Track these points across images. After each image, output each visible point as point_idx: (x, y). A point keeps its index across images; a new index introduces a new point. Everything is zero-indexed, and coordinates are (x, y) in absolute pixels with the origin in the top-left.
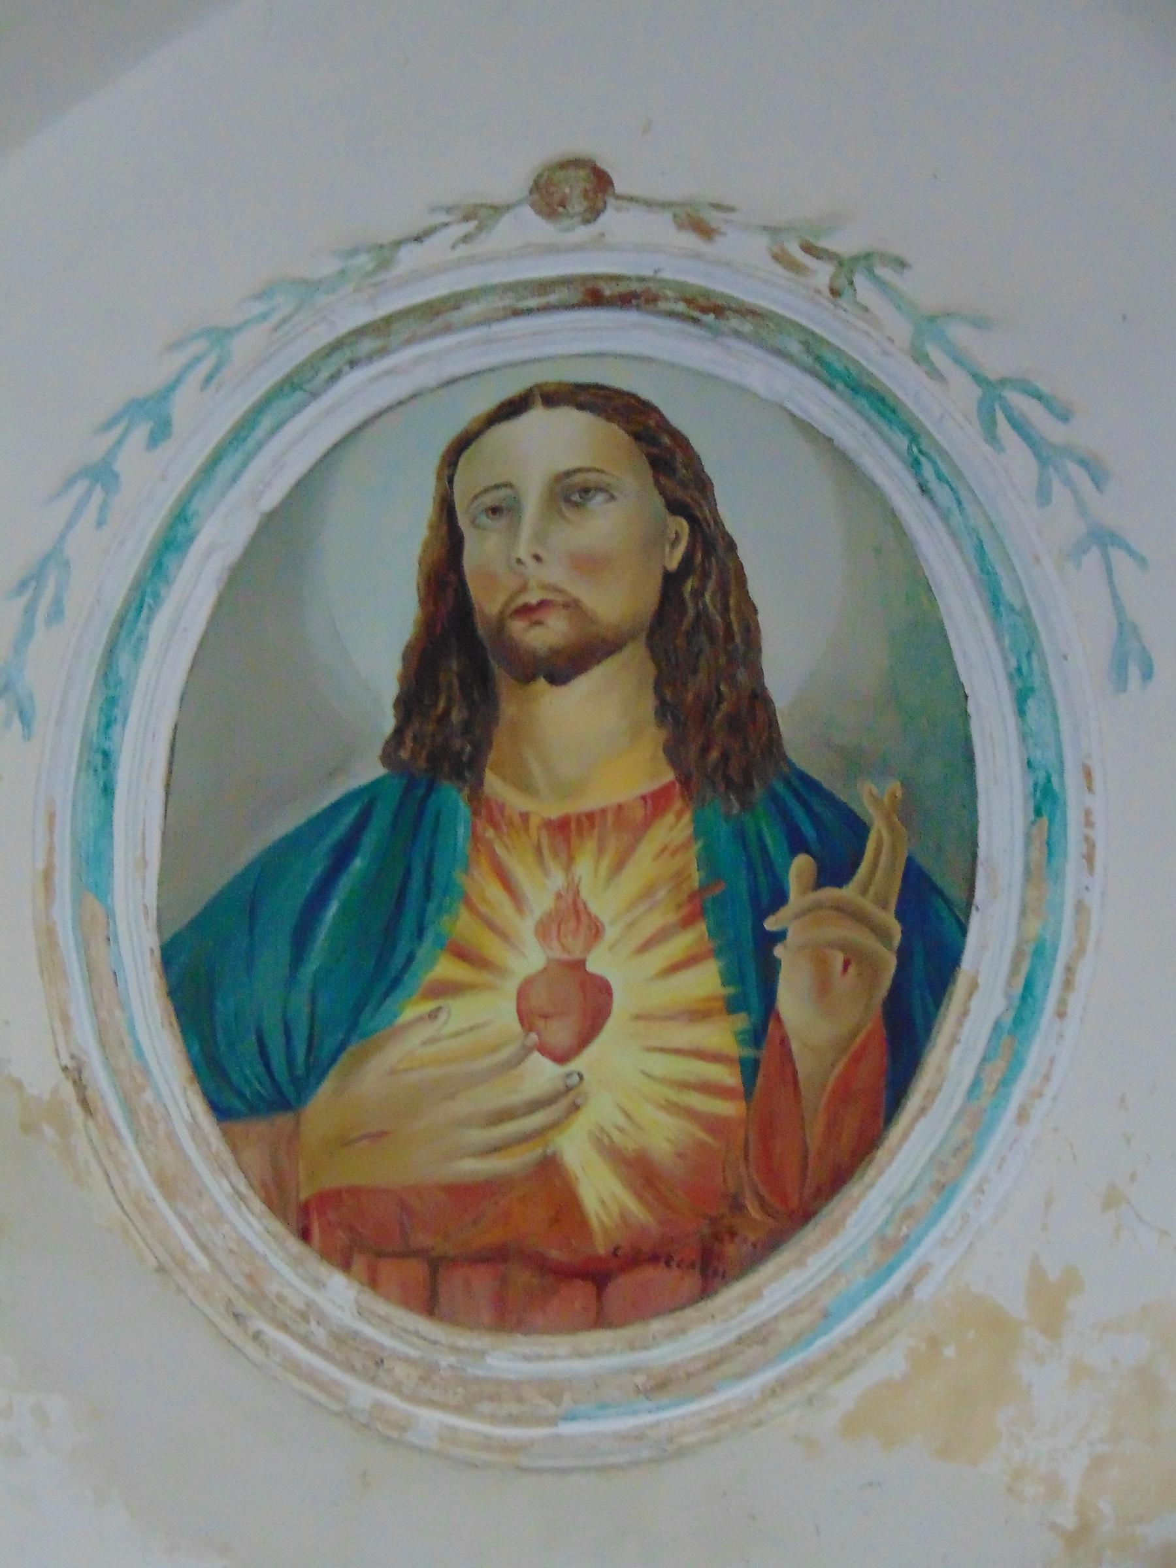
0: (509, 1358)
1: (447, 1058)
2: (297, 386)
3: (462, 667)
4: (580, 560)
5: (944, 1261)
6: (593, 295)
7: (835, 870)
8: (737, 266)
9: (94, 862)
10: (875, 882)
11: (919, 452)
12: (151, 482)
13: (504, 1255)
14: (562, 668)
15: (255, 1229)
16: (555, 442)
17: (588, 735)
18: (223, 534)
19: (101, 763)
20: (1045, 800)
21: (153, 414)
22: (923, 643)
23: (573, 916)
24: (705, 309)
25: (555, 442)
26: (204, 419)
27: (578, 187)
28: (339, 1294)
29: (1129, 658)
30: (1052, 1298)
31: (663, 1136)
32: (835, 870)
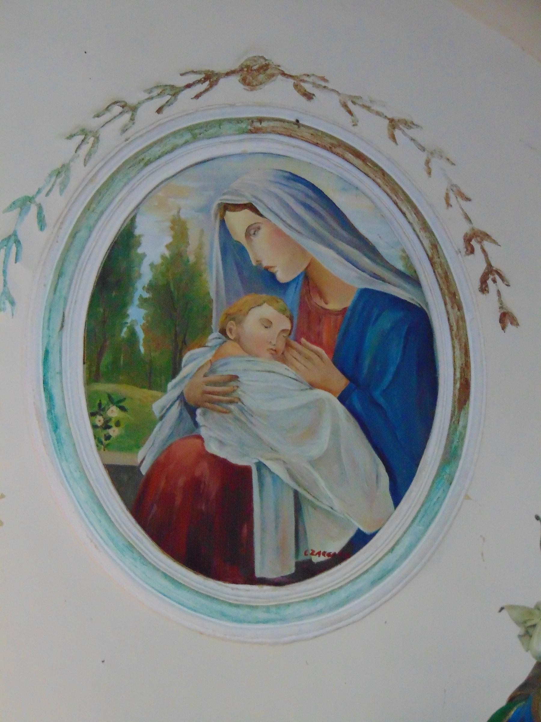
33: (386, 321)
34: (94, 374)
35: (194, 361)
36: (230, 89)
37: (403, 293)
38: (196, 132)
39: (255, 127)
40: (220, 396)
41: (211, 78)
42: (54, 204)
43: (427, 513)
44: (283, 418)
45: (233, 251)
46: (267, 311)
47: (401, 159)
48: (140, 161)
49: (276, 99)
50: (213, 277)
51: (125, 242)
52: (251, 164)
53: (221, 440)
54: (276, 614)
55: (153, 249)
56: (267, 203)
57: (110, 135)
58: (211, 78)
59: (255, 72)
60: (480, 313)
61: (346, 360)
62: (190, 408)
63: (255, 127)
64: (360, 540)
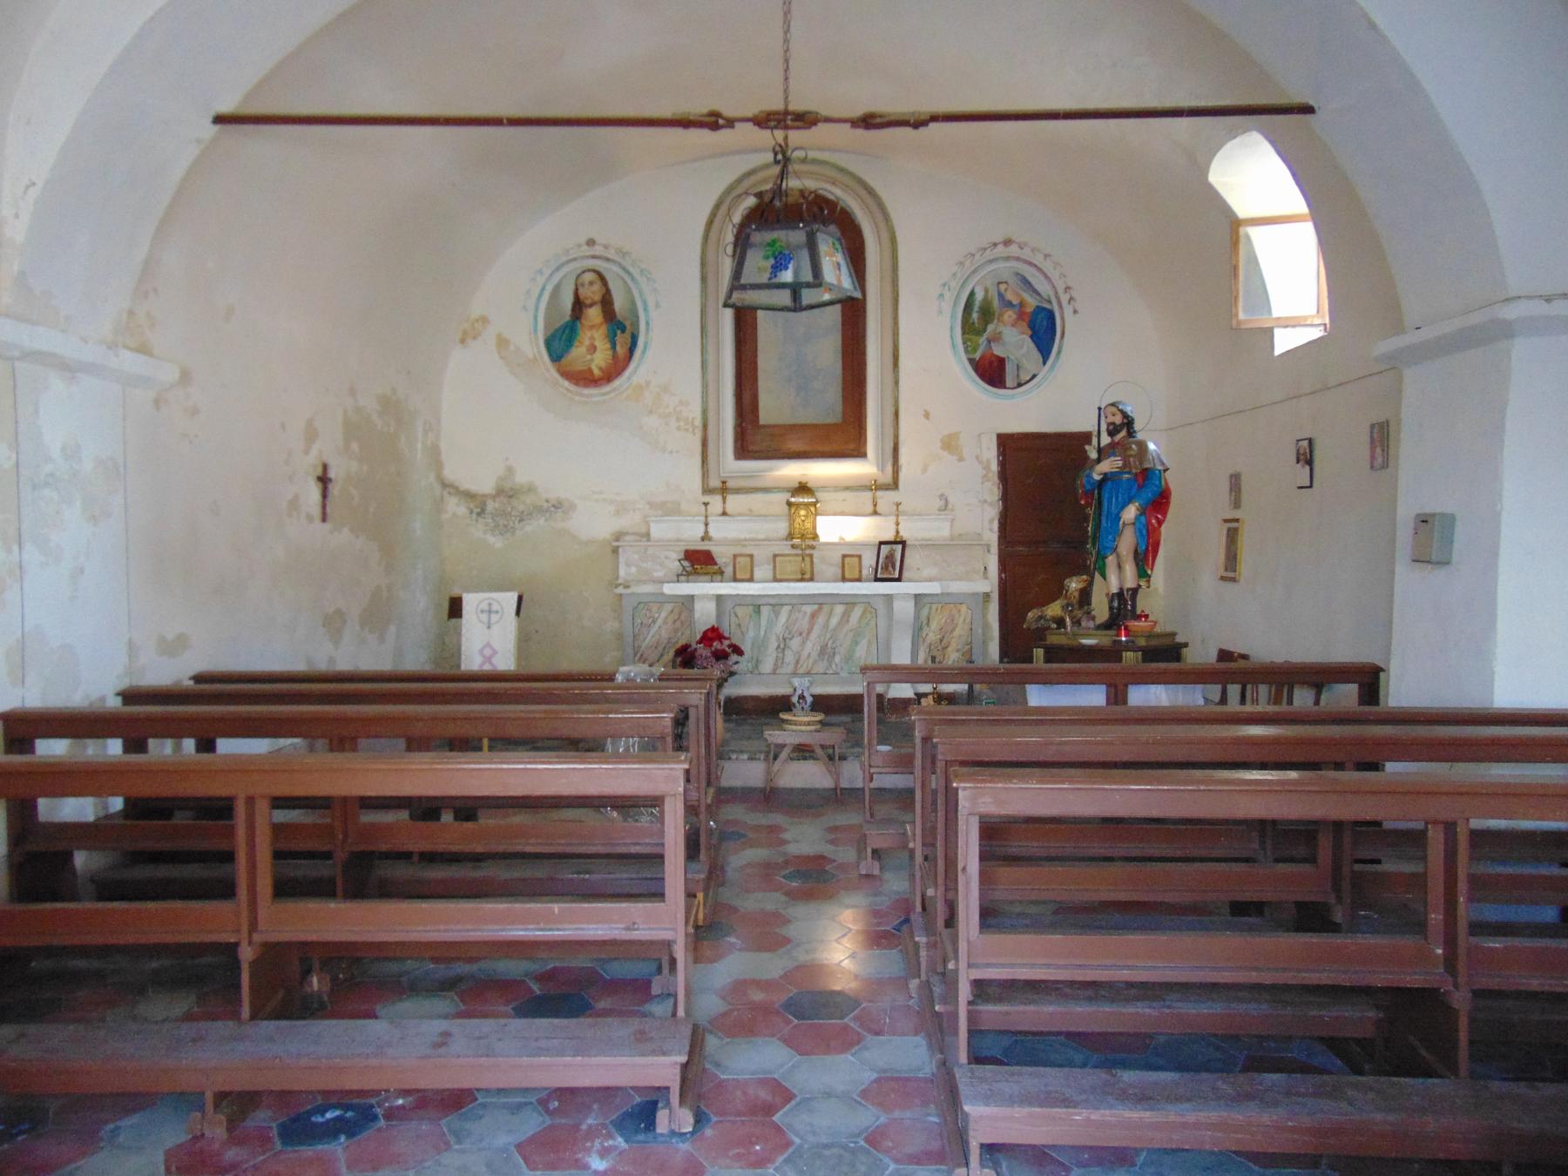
0: (586, 391)
1: (578, 353)
2: (558, 269)
3: (579, 306)
4: (592, 293)
5: (635, 380)
6: (594, 257)
7: (623, 331)
8: (611, 254)
9: (536, 330)
10: (627, 335)
11: (633, 278)
12: (541, 280)
13: (585, 379)
14: (591, 305)
15: (556, 375)
16: (589, 277)
17: (594, 314)
18: (549, 288)
19: (536, 318)
20: (647, 324)
21: (540, 272)
22: (633, 303)
23: (592, 338)
24: (608, 259)
25: (589, 277)
26: (547, 272)
27: (591, 242)
28: (566, 383)
29: (657, 306)
30: (648, 383)
31: (603, 364)
32: (623, 331)
33: (1043, 315)
34: (964, 333)
35: (990, 328)
36: (1000, 248)
37: (1047, 306)
38: (991, 261)
39: (1008, 258)
40: (996, 338)
41: (995, 245)
42: (953, 284)
43: (1053, 366)
44: (1014, 343)
45: (1001, 295)
46: (1010, 313)
47: (1047, 266)
48: (974, 272)
49: (1013, 250)
50: (996, 303)
51: (972, 294)
52: (1005, 269)
53: (998, 351)
54: (1013, 397)
55: (979, 296)
56: (1011, 281)
57: (967, 264)
58: (995, 245)
59: (1007, 242)
60: (1068, 311)
61: (1032, 326)
62: (989, 341)
63: (1008, 258)
64: (1034, 376)
